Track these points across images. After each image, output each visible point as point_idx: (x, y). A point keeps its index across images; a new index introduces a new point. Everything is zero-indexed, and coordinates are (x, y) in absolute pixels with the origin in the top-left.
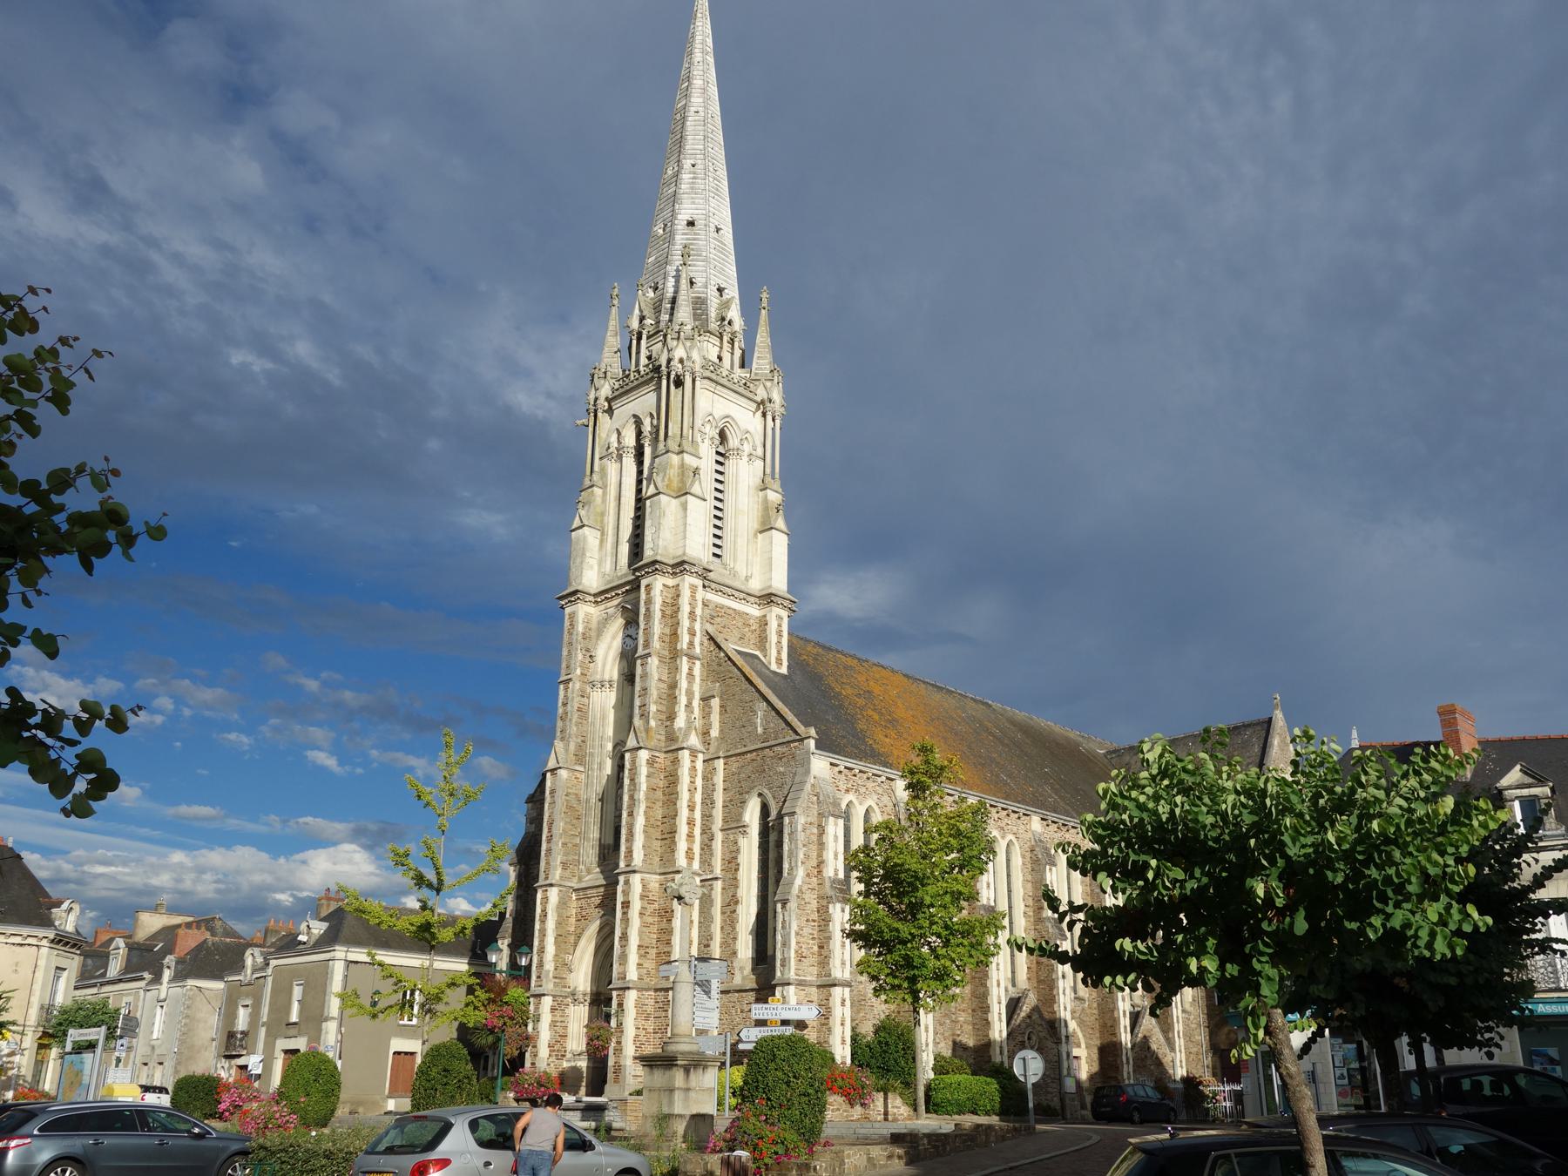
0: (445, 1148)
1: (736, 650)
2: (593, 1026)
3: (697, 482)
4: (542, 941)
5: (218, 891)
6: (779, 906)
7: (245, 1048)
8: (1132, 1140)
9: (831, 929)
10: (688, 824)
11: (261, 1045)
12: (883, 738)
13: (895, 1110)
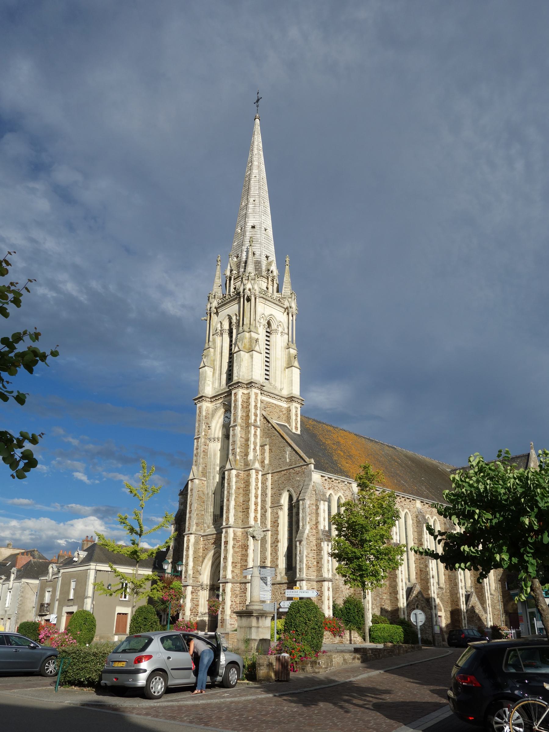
0: (149, 650)
1: (276, 423)
2: (211, 600)
3: (257, 345)
4: (187, 560)
5: (32, 539)
6: (298, 543)
7: (49, 611)
8: (470, 644)
9: (322, 554)
10: (255, 504)
11: (56, 610)
12: (345, 464)
13: (355, 639)
